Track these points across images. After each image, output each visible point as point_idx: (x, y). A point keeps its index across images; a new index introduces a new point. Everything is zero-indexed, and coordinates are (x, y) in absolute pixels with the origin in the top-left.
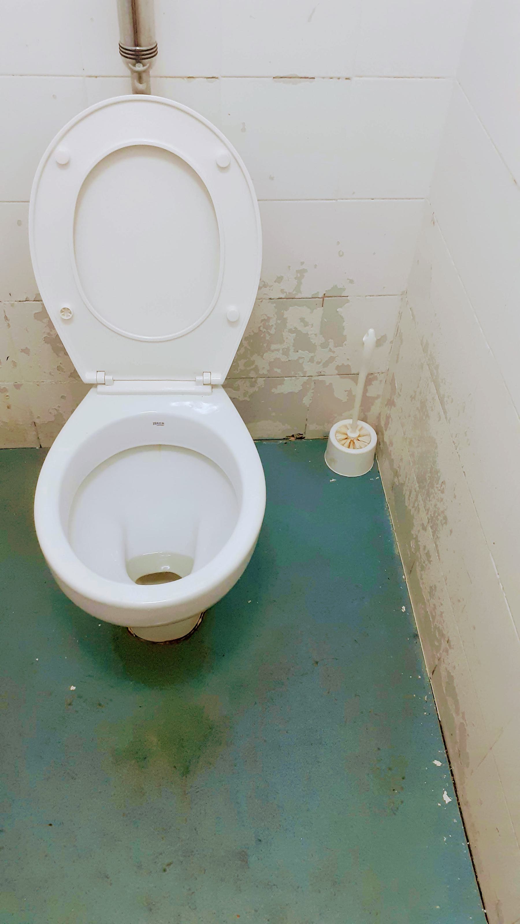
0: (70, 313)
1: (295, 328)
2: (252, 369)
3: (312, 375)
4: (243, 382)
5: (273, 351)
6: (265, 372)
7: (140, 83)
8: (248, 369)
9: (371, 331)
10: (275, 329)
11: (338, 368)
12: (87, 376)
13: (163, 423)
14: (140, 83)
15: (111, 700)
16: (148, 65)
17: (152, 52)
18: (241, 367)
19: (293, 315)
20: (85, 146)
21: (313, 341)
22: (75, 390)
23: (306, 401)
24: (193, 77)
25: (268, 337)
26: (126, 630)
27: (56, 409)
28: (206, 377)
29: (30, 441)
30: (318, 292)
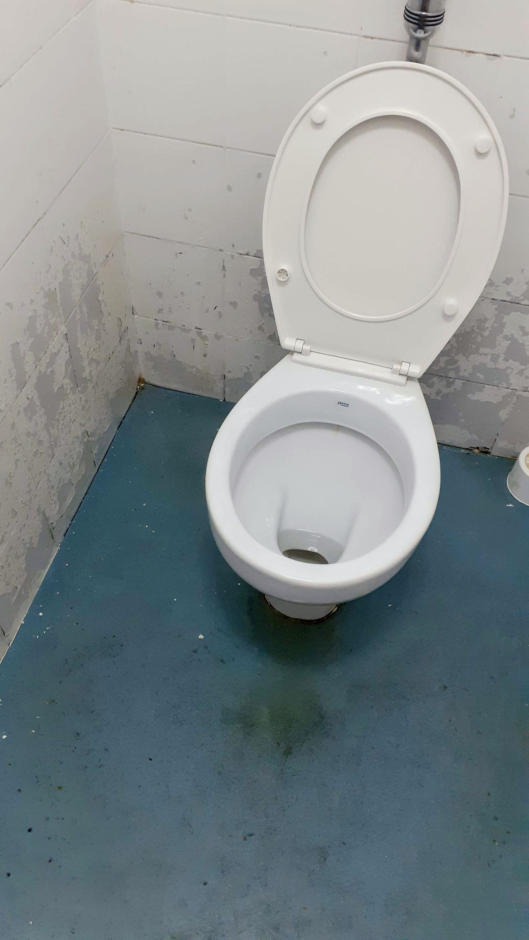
0: (287, 275)
1: (512, 335)
2: (453, 369)
3: (517, 388)
4: (440, 379)
5: (481, 354)
6: (466, 374)
7: (416, 51)
8: (449, 367)
10: (490, 331)
12: (287, 342)
13: (348, 405)
14: (416, 51)
15: (234, 660)
16: (430, 33)
17: (438, 19)
18: (442, 364)
20: (341, 110)
22: (272, 352)
23: (503, 414)
24: (473, 52)
25: (479, 339)
26: (262, 596)
27: (247, 367)
28: (405, 367)
29: (216, 392)
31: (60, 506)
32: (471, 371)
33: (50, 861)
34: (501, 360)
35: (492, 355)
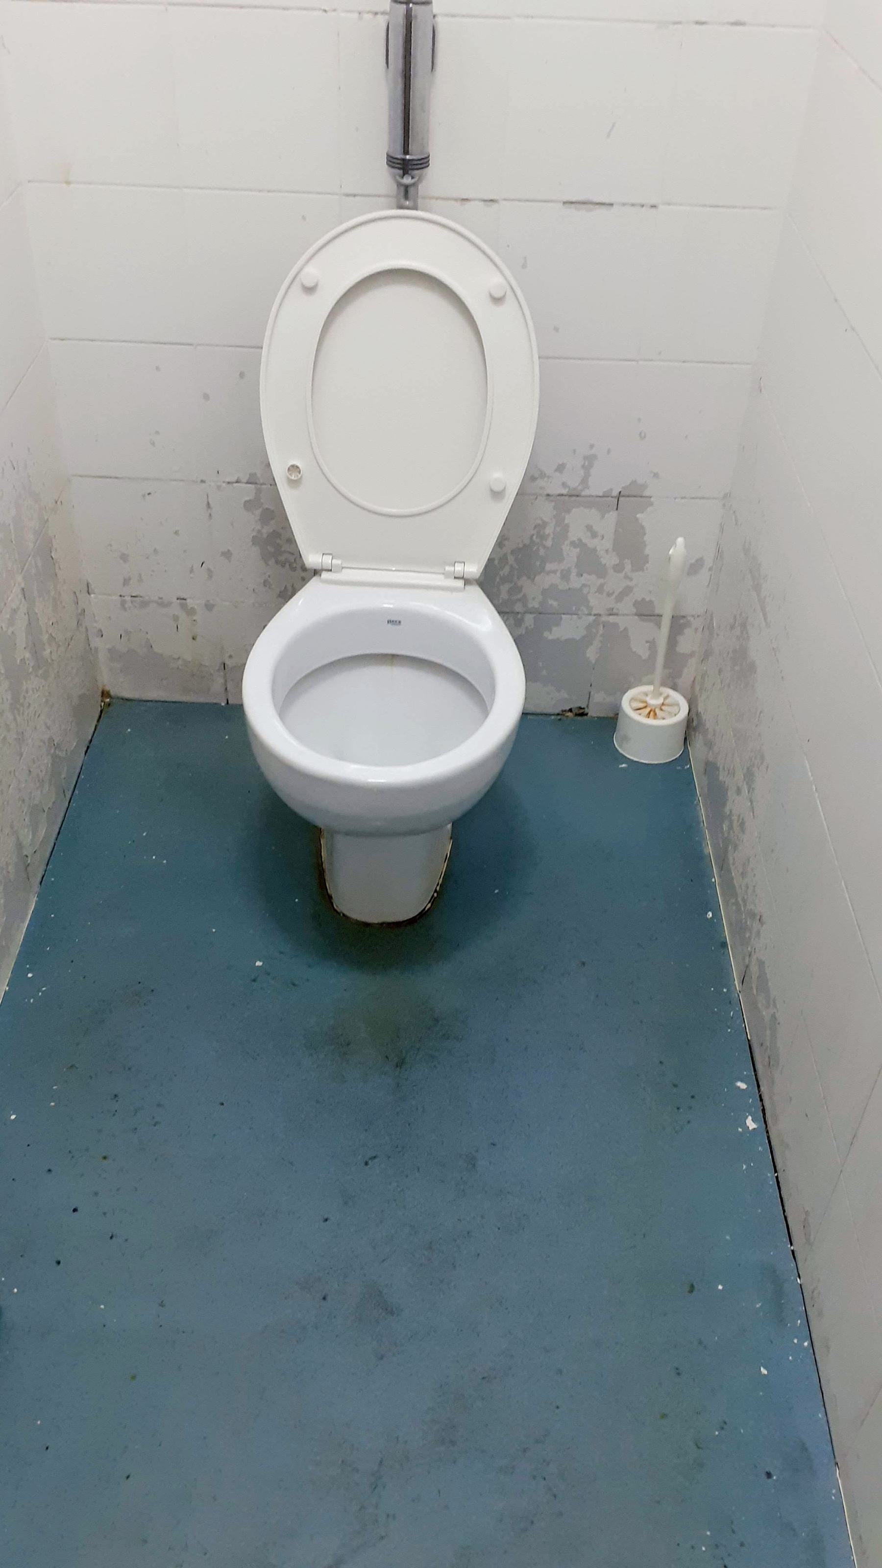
1: (580, 540)
2: (519, 600)
5: (548, 573)
9: (680, 540)
11: (636, 604)
12: (312, 559)
14: (406, 196)
17: (423, 163)
19: (578, 520)
20: (339, 266)
21: (603, 561)
23: (592, 654)
25: (542, 552)
28: (459, 568)
30: (611, 490)
31: (34, 834)
32: (540, 598)
33: (111, 1238)
34: (573, 575)
35: (562, 571)
